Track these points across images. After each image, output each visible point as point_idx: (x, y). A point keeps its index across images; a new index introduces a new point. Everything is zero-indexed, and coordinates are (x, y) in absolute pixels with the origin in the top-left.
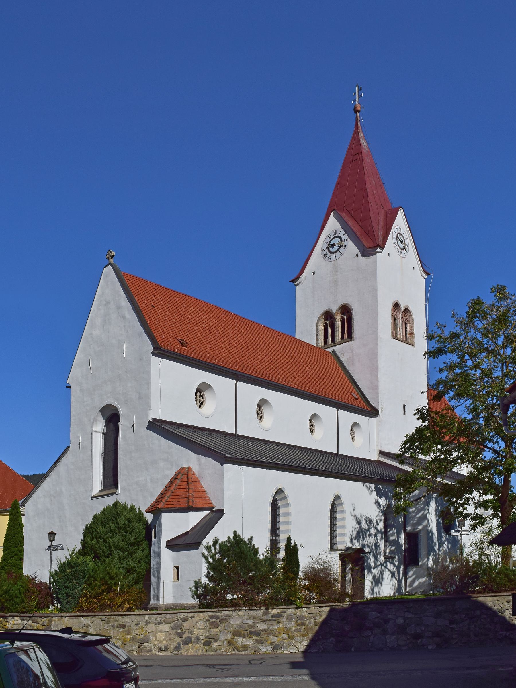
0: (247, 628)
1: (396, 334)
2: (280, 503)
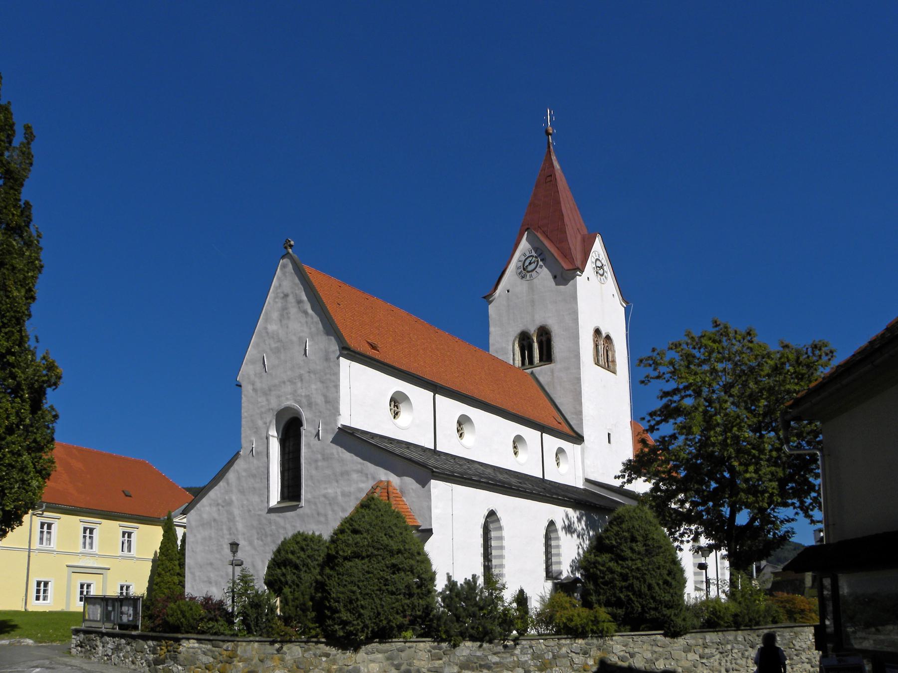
0: (476, 661)
1: (598, 360)
2: (491, 526)
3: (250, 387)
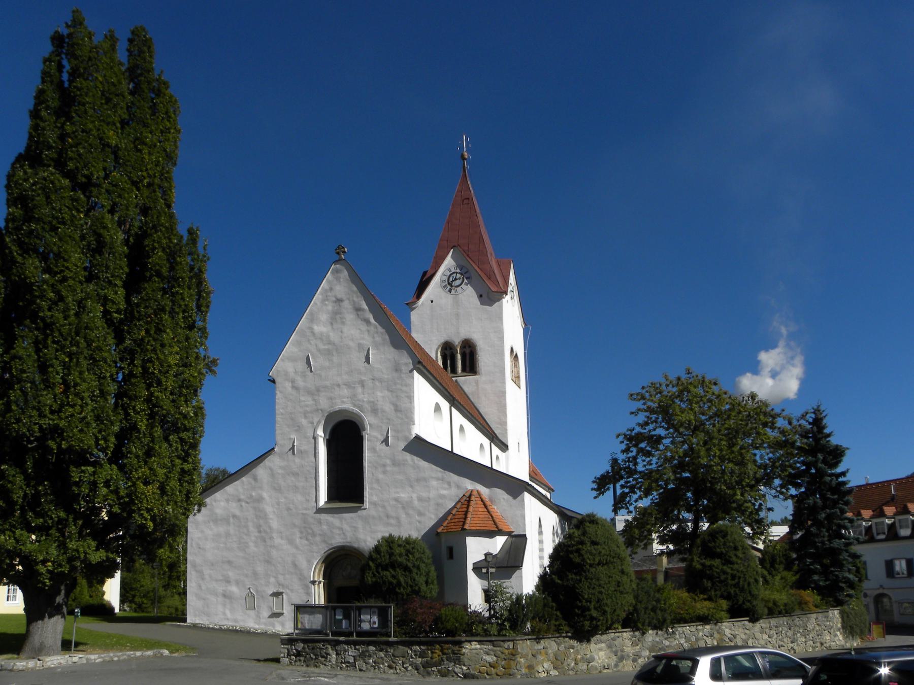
3: (288, 385)
